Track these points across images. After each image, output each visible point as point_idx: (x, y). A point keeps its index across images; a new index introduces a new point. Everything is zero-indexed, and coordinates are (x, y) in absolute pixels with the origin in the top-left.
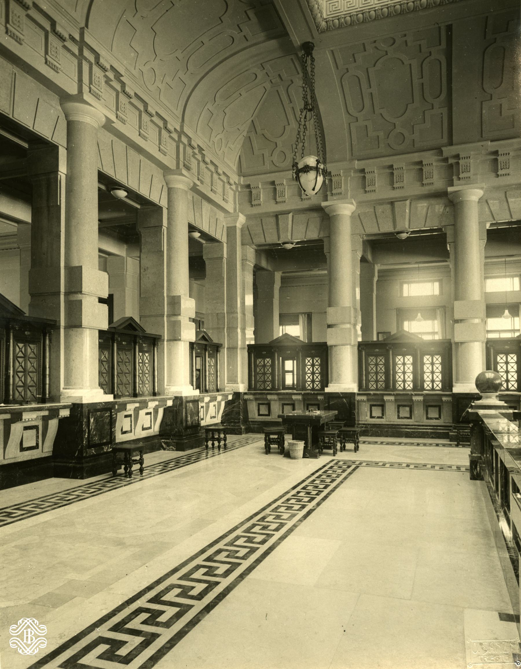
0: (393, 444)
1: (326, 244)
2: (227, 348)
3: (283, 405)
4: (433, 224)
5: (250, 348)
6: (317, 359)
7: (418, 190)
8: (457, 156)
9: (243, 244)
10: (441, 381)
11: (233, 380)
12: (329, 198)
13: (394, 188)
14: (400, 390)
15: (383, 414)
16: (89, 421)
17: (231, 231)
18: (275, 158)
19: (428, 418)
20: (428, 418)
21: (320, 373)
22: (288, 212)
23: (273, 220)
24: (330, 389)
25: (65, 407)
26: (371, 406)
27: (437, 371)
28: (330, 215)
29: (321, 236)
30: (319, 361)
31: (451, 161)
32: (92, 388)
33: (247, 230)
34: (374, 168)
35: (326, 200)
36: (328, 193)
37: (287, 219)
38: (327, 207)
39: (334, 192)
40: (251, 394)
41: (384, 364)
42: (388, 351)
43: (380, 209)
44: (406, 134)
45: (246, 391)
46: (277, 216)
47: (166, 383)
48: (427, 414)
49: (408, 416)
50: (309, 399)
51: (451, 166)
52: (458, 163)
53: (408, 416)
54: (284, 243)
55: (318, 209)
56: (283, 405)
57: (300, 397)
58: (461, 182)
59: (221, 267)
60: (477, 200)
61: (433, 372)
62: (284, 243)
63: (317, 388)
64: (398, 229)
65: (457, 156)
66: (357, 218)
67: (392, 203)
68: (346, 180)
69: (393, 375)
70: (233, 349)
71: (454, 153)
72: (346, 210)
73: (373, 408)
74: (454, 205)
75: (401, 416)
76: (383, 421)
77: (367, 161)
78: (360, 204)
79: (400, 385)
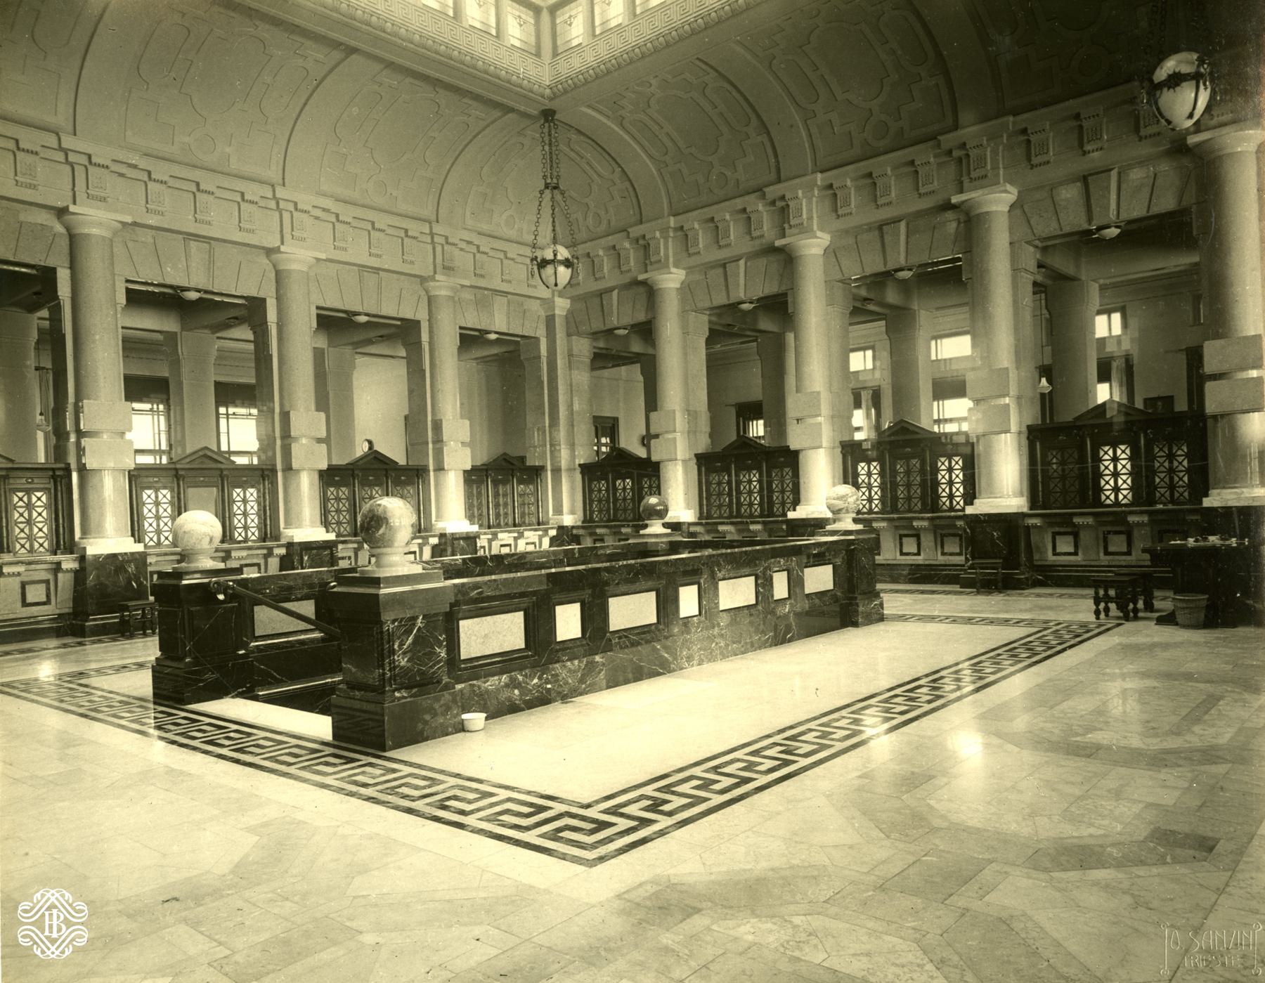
0: (933, 592)
1: (790, 299)
2: (474, 477)
3: (901, 537)
4: (1166, 203)
5: (585, 469)
6: (1123, 447)
7: (747, 246)
8: (783, 198)
9: (569, 335)
10: (1131, 489)
11: (558, 510)
12: (787, 231)
13: (878, 207)
14: (1109, 506)
15: (1076, 546)
16: (302, 559)
17: (550, 321)
18: (590, 221)
19: (902, 554)
20: (902, 554)
21: (1130, 474)
22: (896, 221)
23: (597, 300)
24: (982, 506)
25: (282, 546)
26: (1055, 535)
27: (165, 514)
28: (972, 214)
29: (784, 288)
30: (1128, 451)
31: (956, 153)
32: (313, 525)
33: (570, 317)
34: (694, 223)
35: (783, 236)
36: (786, 226)
37: (738, 267)
38: (963, 202)
39: (973, 175)
40: (732, 523)
41: (1154, 457)
42: (923, 450)
43: (712, 273)
44: (729, 173)
45: (579, 523)
46: (880, 228)
47: (282, 525)
48: (942, 547)
49: (1125, 550)
50: (943, 527)
51: (960, 160)
52: (968, 156)
53: (1125, 550)
54: (1100, 228)
55: (772, 250)
56: (901, 537)
57: (925, 524)
58: (794, 231)
59: (539, 369)
60: (1007, 209)
61: (245, 514)
62: (1100, 228)
63: (1125, 501)
64: (890, 266)
65: (783, 198)
66: (832, 253)
67: (724, 266)
68: (809, 203)
69: (1093, 479)
70: (557, 471)
71: (780, 194)
72: (671, 280)
73: (905, 540)
74: (787, 260)
75: (905, 550)
76: (920, 560)
77: (835, 172)
78: (690, 270)
79: (1108, 496)
